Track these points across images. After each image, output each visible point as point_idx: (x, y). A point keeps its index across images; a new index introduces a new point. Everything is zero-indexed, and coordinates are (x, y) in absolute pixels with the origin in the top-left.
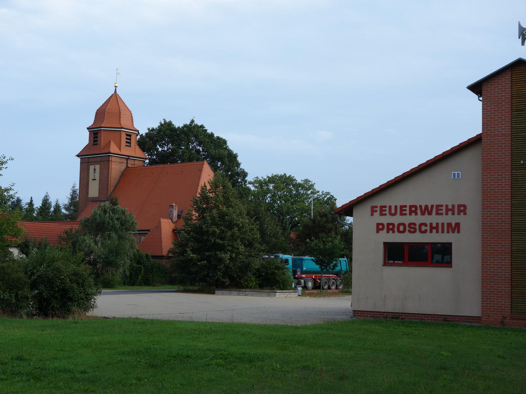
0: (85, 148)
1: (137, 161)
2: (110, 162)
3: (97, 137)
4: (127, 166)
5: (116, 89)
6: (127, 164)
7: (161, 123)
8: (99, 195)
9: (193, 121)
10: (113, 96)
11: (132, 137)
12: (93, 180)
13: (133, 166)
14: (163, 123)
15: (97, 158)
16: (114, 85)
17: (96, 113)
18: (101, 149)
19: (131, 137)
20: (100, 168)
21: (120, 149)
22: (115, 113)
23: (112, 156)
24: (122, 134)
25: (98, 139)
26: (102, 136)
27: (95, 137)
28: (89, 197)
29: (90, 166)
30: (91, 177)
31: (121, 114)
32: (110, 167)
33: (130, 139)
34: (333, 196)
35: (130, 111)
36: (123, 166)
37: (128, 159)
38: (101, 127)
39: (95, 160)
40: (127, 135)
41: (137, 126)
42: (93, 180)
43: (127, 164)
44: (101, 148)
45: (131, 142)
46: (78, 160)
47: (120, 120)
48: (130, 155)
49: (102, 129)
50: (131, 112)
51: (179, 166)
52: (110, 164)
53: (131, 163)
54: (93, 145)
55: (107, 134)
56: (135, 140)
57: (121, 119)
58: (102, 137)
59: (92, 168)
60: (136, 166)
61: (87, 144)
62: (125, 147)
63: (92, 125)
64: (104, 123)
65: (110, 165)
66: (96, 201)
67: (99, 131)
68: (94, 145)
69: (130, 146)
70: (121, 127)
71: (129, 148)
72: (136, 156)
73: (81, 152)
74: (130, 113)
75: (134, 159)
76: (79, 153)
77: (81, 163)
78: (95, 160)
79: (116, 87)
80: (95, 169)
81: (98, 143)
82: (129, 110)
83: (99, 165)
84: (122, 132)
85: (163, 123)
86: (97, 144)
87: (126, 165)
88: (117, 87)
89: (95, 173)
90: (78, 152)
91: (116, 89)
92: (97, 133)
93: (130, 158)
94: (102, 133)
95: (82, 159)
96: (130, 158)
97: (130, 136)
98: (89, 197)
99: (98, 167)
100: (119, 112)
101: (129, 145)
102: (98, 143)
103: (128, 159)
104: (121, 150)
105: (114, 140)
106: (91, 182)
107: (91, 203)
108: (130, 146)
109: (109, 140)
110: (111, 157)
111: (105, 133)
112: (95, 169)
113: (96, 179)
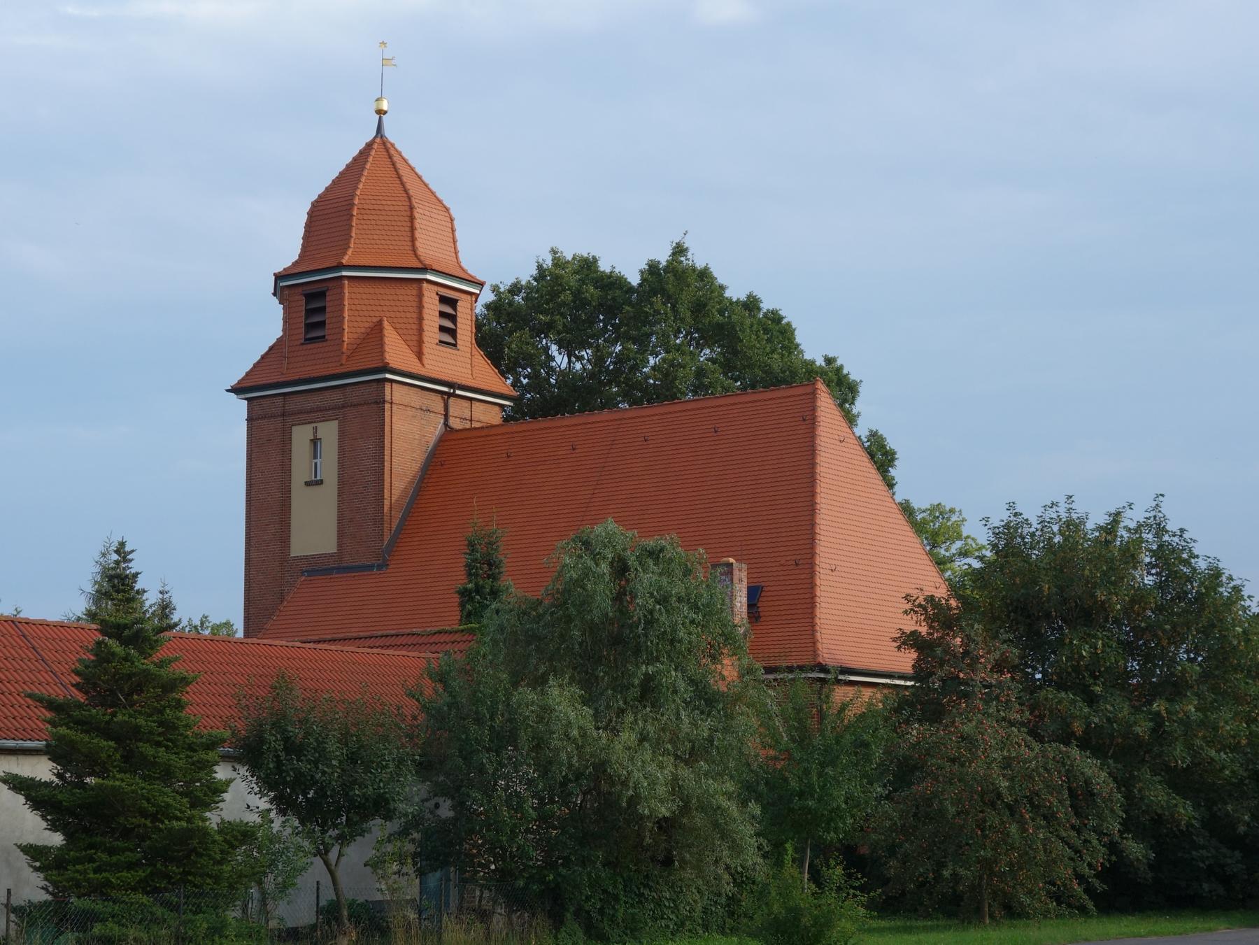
0: (263, 357)
1: (481, 406)
2: (387, 406)
3: (322, 310)
4: (446, 424)
5: (380, 119)
6: (446, 416)
7: (540, 267)
8: (340, 545)
9: (679, 250)
10: (375, 146)
11: (459, 308)
12: (308, 484)
13: (468, 426)
14: (549, 263)
15: (327, 394)
16: (374, 107)
17: (311, 214)
18: (344, 357)
19: (455, 309)
20: (342, 435)
21: (420, 355)
22: (393, 213)
23: (392, 381)
24: (426, 293)
25: (328, 317)
26: (346, 303)
27: (310, 309)
28: (293, 554)
29: (294, 428)
30: (300, 469)
31: (416, 215)
32: (387, 428)
33: (453, 318)
34: (465, 594)
35: (445, 207)
36: (434, 429)
37: (449, 398)
38: (341, 267)
39: (314, 401)
40: (444, 300)
41: (471, 262)
42: (308, 484)
43: (446, 416)
44: (343, 353)
45: (459, 331)
46: (240, 407)
47: (413, 239)
48: (459, 382)
49: (344, 273)
50: (447, 210)
51: (694, 410)
52: (387, 414)
53: (460, 414)
54: (302, 344)
55: (364, 296)
56: (469, 323)
57: (417, 235)
58: (346, 308)
59: (301, 436)
60: (475, 425)
61: (271, 344)
62: (438, 347)
63: (294, 264)
64: (350, 252)
65: (387, 420)
66: (327, 571)
67: (330, 285)
68: (309, 340)
69: (455, 345)
70: (420, 266)
71: (448, 350)
72: (476, 386)
73: (247, 374)
74: (447, 214)
75: (471, 399)
76: (243, 379)
77: (249, 420)
78: (314, 401)
79: (380, 112)
80: (315, 442)
81: (326, 332)
82: (440, 201)
83: (337, 422)
84: (425, 285)
85: (549, 263)
86: (324, 337)
87: (442, 421)
88: (385, 112)
89: (315, 457)
90: (237, 373)
91: (380, 119)
92: (321, 295)
93: (458, 392)
94: (346, 291)
95: (255, 403)
96: (458, 392)
97: (452, 303)
98: (293, 554)
99: (329, 431)
100: (407, 208)
101: (453, 342)
102: (326, 332)
103: (449, 395)
104: (426, 361)
105: (395, 320)
106: (300, 497)
107: (303, 578)
108: (455, 345)
109: (375, 320)
110: (387, 386)
111: (356, 290)
112: (315, 442)
113: (321, 482)
